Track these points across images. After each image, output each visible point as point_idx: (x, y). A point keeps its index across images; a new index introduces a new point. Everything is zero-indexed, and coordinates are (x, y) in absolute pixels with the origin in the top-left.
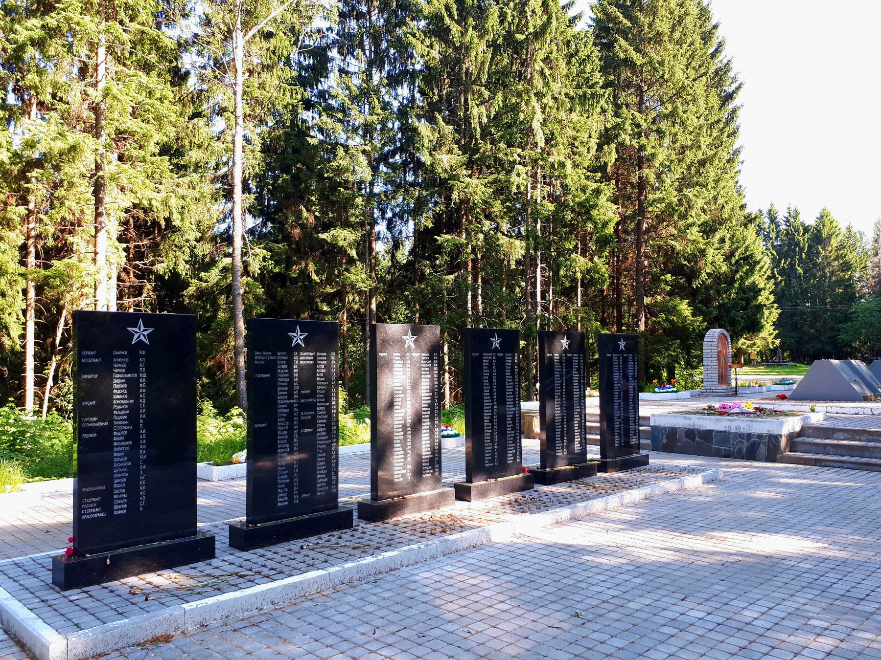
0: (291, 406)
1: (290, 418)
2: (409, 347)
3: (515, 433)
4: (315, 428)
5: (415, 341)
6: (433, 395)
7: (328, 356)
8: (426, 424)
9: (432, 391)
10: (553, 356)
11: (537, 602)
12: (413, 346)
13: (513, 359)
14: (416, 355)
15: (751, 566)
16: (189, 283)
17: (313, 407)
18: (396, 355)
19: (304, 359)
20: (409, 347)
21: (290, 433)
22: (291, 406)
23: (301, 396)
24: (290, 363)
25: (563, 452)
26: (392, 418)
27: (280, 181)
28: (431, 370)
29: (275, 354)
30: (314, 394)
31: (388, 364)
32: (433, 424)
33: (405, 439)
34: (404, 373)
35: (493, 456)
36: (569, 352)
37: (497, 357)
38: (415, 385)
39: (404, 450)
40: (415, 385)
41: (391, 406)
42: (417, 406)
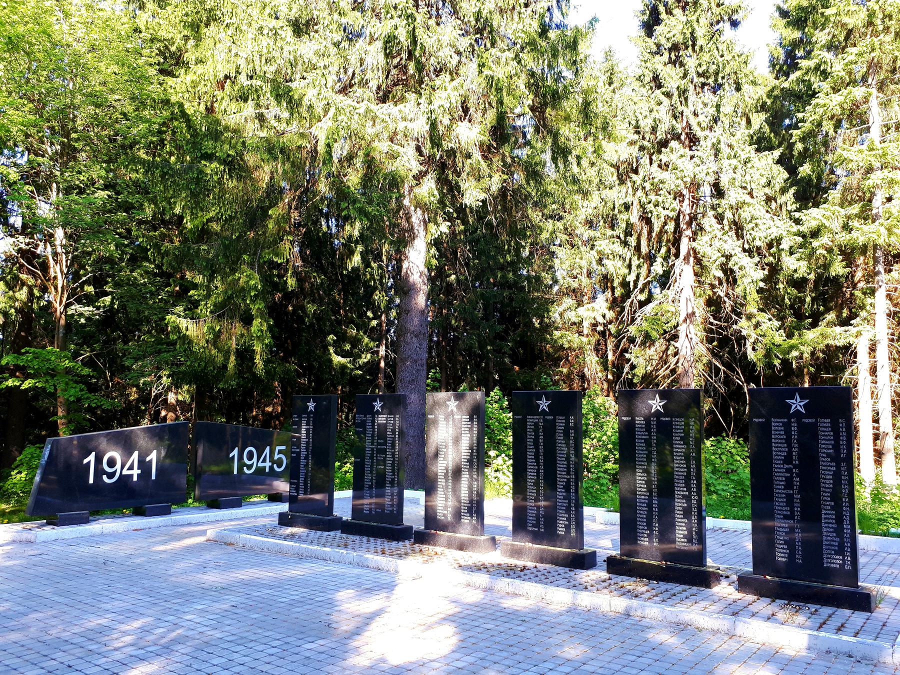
0: (372, 449)
1: (371, 458)
2: (452, 411)
3: (569, 503)
4: (385, 466)
5: (457, 406)
6: (472, 452)
7: (395, 418)
8: (465, 476)
9: (471, 448)
10: (633, 420)
11: (490, 616)
12: (455, 410)
13: (567, 422)
14: (457, 417)
15: (423, 437)
16: (220, 317)
17: (384, 452)
18: (441, 417)
19: (381, 419)
20: (452, 411)
21: (372, 466)
22: (372, 449)
23: (379, 444)
24: (373, 422)
25: (651, 541)
26: (437, 467)
27: (370, 314)
28: (471, 429)
29: (365, 416)
30: (385, 444)
31: (435, 422)
32: (471, 477)
33: (447, 486)
34: (447, 432)
35: (538, 520)
36: (665, 415)
37: (545, 420)
38: (457, 440)
39: (445, 494)
40: (457, 440)
41: (436, 455)
42: (457, 459)
